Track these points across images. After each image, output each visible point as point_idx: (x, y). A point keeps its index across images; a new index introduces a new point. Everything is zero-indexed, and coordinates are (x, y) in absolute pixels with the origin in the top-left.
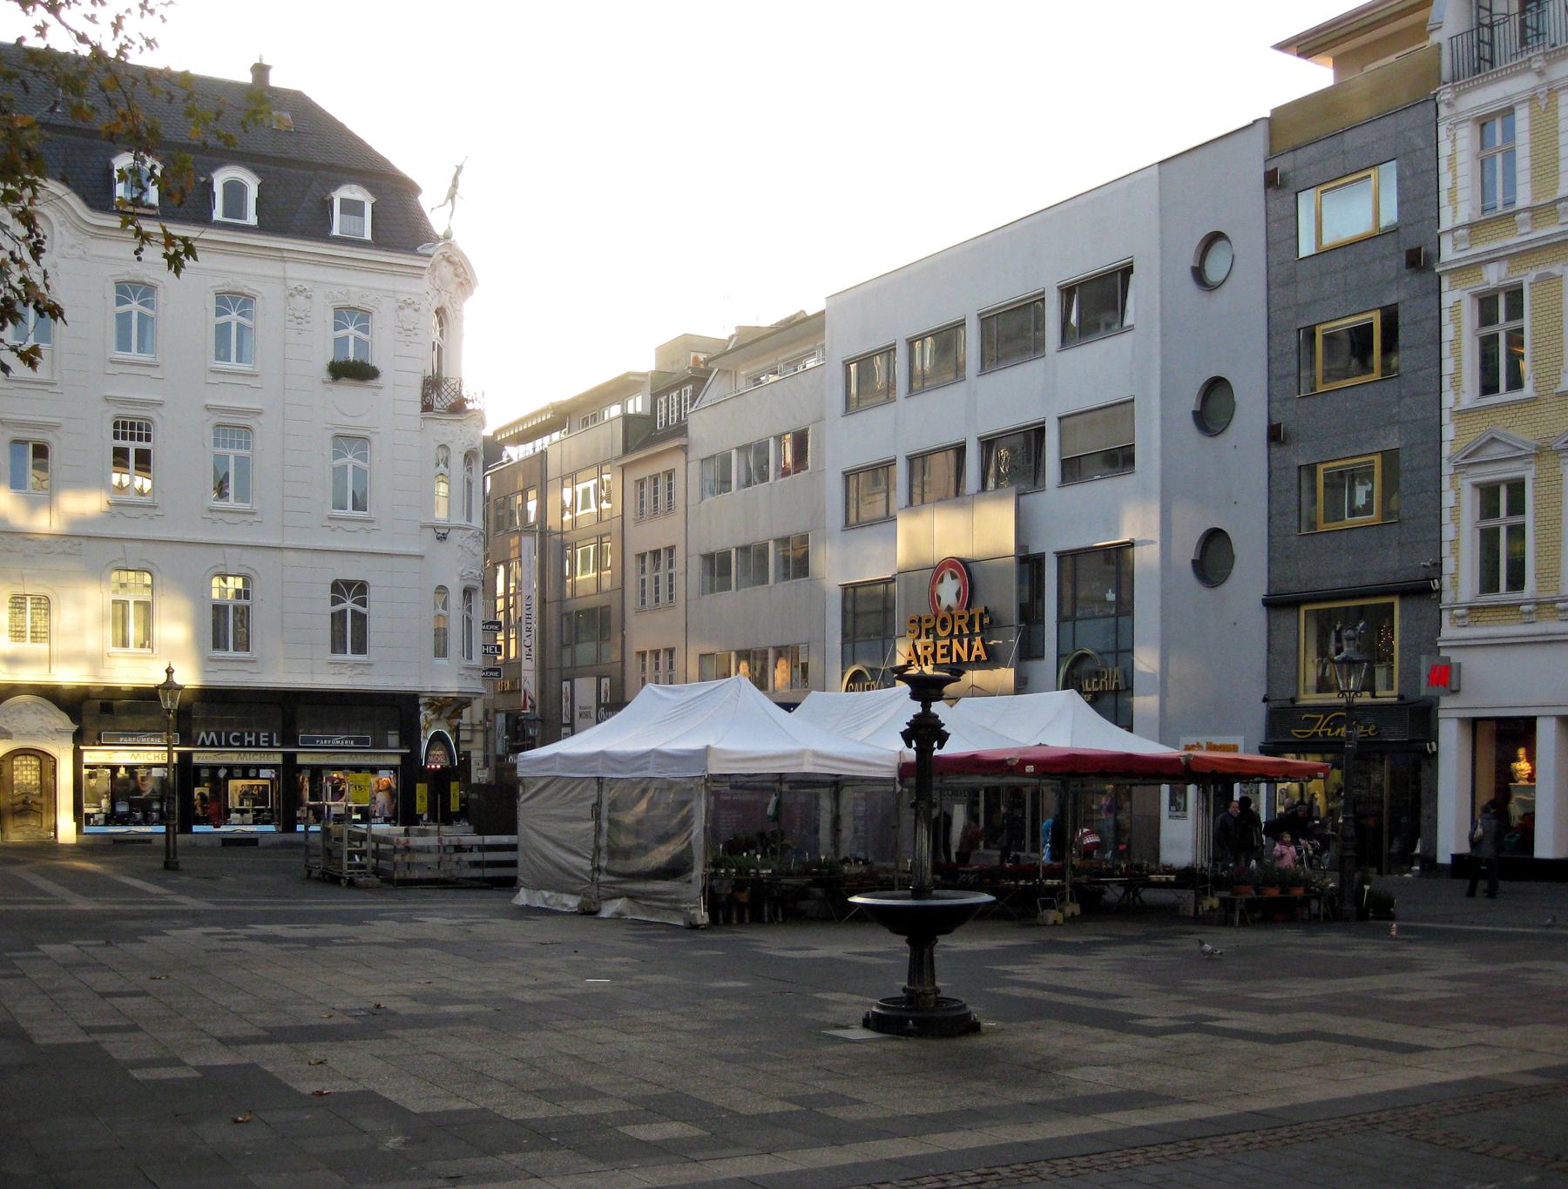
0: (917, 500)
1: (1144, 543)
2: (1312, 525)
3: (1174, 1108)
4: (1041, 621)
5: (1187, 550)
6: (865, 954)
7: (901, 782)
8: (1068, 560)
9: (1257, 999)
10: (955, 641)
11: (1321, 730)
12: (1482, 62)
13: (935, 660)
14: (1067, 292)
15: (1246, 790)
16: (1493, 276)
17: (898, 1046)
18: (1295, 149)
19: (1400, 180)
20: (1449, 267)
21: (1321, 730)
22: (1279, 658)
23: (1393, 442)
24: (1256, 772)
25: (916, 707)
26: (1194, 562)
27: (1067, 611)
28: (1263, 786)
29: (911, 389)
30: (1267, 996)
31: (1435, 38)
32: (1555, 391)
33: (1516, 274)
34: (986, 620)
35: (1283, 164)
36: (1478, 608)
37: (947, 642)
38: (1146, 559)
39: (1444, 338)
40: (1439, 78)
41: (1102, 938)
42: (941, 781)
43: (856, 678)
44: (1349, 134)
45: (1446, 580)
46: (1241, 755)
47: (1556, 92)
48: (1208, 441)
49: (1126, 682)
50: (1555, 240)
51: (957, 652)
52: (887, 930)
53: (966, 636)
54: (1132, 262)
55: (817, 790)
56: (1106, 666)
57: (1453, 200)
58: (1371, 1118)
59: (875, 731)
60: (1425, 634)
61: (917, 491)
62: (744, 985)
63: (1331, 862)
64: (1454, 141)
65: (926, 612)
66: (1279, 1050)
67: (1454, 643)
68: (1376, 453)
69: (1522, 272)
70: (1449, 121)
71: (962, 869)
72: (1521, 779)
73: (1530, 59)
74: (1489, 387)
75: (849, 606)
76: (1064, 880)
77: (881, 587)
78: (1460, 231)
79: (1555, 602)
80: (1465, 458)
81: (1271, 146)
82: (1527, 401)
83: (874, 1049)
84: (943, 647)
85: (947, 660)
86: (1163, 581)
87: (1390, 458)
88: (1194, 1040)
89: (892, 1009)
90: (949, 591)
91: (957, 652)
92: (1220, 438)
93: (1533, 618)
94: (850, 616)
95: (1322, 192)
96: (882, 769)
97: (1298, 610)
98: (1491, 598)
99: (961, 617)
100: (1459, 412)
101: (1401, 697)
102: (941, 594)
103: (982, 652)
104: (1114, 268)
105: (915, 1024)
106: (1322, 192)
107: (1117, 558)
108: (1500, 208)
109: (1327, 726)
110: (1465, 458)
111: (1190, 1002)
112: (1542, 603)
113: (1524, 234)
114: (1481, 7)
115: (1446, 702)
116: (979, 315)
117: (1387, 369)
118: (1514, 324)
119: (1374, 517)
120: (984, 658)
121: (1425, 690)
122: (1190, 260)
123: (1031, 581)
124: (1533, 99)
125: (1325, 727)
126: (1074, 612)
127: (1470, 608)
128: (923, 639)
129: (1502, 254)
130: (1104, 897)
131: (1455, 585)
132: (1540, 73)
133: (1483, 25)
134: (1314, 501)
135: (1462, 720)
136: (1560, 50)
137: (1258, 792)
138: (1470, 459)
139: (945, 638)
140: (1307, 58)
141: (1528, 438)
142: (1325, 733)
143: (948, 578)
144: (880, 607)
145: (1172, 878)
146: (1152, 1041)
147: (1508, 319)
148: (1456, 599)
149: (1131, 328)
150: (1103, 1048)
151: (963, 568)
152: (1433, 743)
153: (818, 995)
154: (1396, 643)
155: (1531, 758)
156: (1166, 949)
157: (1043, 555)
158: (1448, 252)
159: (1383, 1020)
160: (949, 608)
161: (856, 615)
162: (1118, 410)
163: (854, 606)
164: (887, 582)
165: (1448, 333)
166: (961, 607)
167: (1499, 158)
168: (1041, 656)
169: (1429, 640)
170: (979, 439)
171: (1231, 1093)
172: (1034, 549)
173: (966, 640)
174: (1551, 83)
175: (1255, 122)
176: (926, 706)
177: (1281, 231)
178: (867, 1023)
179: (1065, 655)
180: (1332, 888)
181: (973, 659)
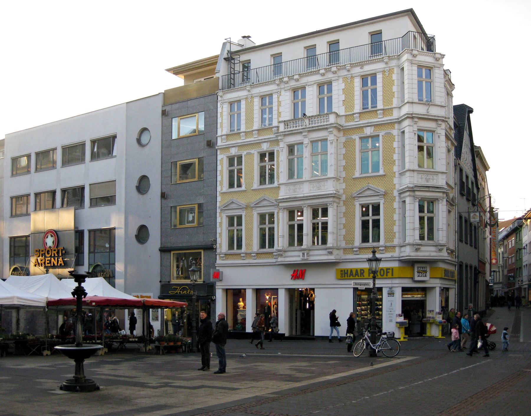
0: (38, 207)
1: (119, 228)
2: (175, 226)
3: (175, 409)
4: (83, 253)
5: (134, 231)
6: (41, 366)
7: (47, 308)
8: (92, 233)
9: (180, 377)
10: (52, 258)
11: (179, 292)
12: (231, 85)
13: (45, 265)
14: (93, 142)
15: (154, 311)
16: (233, 151)
17: (75, 395)
18: (172, 104)
19: (205, 118)
20: (220, 147)
21: (179, 292)
22: (164, 268)
23: (201, 201)
24: (164, 305)
25: (77, 284)
26: (136, 235)
27: (92, 250)
28: (159, 310)
29: (36, 168)
30: (183, 376)
31: (217, 75)
32: (252, 189)
33: (240, 151)
34: (64, 252)
35: (168, 108)
36: (228, 254)
37: (49, 259)
38: (120, 234)
39: (406, 215)
40: (218, 87)
41: (118, 360)
42: (57, 307)
43: (15, 270)
44: (190, 101)
45: (218, 245)
46: (152, 299)
47: (254, 97)
48: (140, 196)
49: (113, 273)
50: (252, 142)
51: (53, 262)
52: (67, 357)
53: (56, 257)
54: (116, 134)
55: (11, 310)
56: (105, 269)
57: (221, 126)
58: (233, 408)
59: (38, 289)
60: (212, 262)
61: (38, 204)
62: (8, 378)
63: (182, 334)
64: (222, 108)
65: (42, 248)
66: (195, 391)
67: (220, 265)
68: (196, 204)
69: (242, 151)
70: (221, 102)
71: (67, 337)
72: (241, 308)
73: (246, 86)
74: (231, 185)
75: (12, 244)
76: (102, 340)
77: (24, 238)
78: (224, 137)
79: (251, 254)
80: (224, 207)
81: (164, 103)
82: (243, 191)
83: (66, 396)
84: (48, 260)
85: (49, 265)
86: (125, 241)
87: (200, 206)
88: (169, 390)
89: (70, 383)
90: (50, 241)
91: (53, 262)
92: (145, 196)
93: (244, 258)
94: (12, 248)
95: (180, 119)
96: (42, 303)
97: (171, 253)
98: (231, 252)
99: (55, 250)
100: (222, 193)
101: (204, 282)
102: (47, 242)
103: (62, 263)
104: (110, 136)
105: (79, 388)
106: (180, 119)
107: (109, 233)
108: (236, 130)
109: (180, 290)
110: (224, 207)
111: (161, 378)
112: (248, 254)
113: (243, 140)
114: (231, 68)
115: (218, 284)
116: (62, 147)
117: (199, 177)
118: (239, 167)
119: (195, 224)
120: (63, 264)
121: (212, 280)
122: (136, 136)
123: (79, 238)
124: (246, 99)
125: (180, 291)
126: (94, 250)
127: (225, 254)
128: (41, 257)
129: (236, 145)
130: (113, 346)
131: (221, 247)
132: (249, 91)
133: (232, 74)
134: (176, 218)
135: (223, 289)
136: (255, 85)
137: (158, 311)
138: (225, 208)
139: (49, 257)
140: (176, 75)
141: (243, 203)
142: (180, 293)
143: (49, 237)
144: (24, 244)
145: (137, 339)
146: (155, 390)
147: (238, 165)
148: (221, 251)
149: (115, 156)
150: (142, 393)
151: (55, 233)
152: (214, 297)
153: (37, 380)
154: (202, 264)
155: (244, 300)
156: (142, 362)
157: (84, 230)
158: (219, 143)
159: (222, 381)
160: (50, 247)
161: (15, 247)
162: (111, 183)
163: (14, 244)
164: (27, 237)
165: (219, 168)
166: (54, 247)
167: (236, 115)
168: (83, 265)
169: (212, 264)
170: (61, 189)
171: (189, 404)
172: (81, 228)
173: (56, 258)
174: (251, 94)
175: (159, 93)
176: (80, 284)
177: (167, 130)
178: (61, 388)
179: (91, 265)
180: (189, 342)
181: (59, 265)
